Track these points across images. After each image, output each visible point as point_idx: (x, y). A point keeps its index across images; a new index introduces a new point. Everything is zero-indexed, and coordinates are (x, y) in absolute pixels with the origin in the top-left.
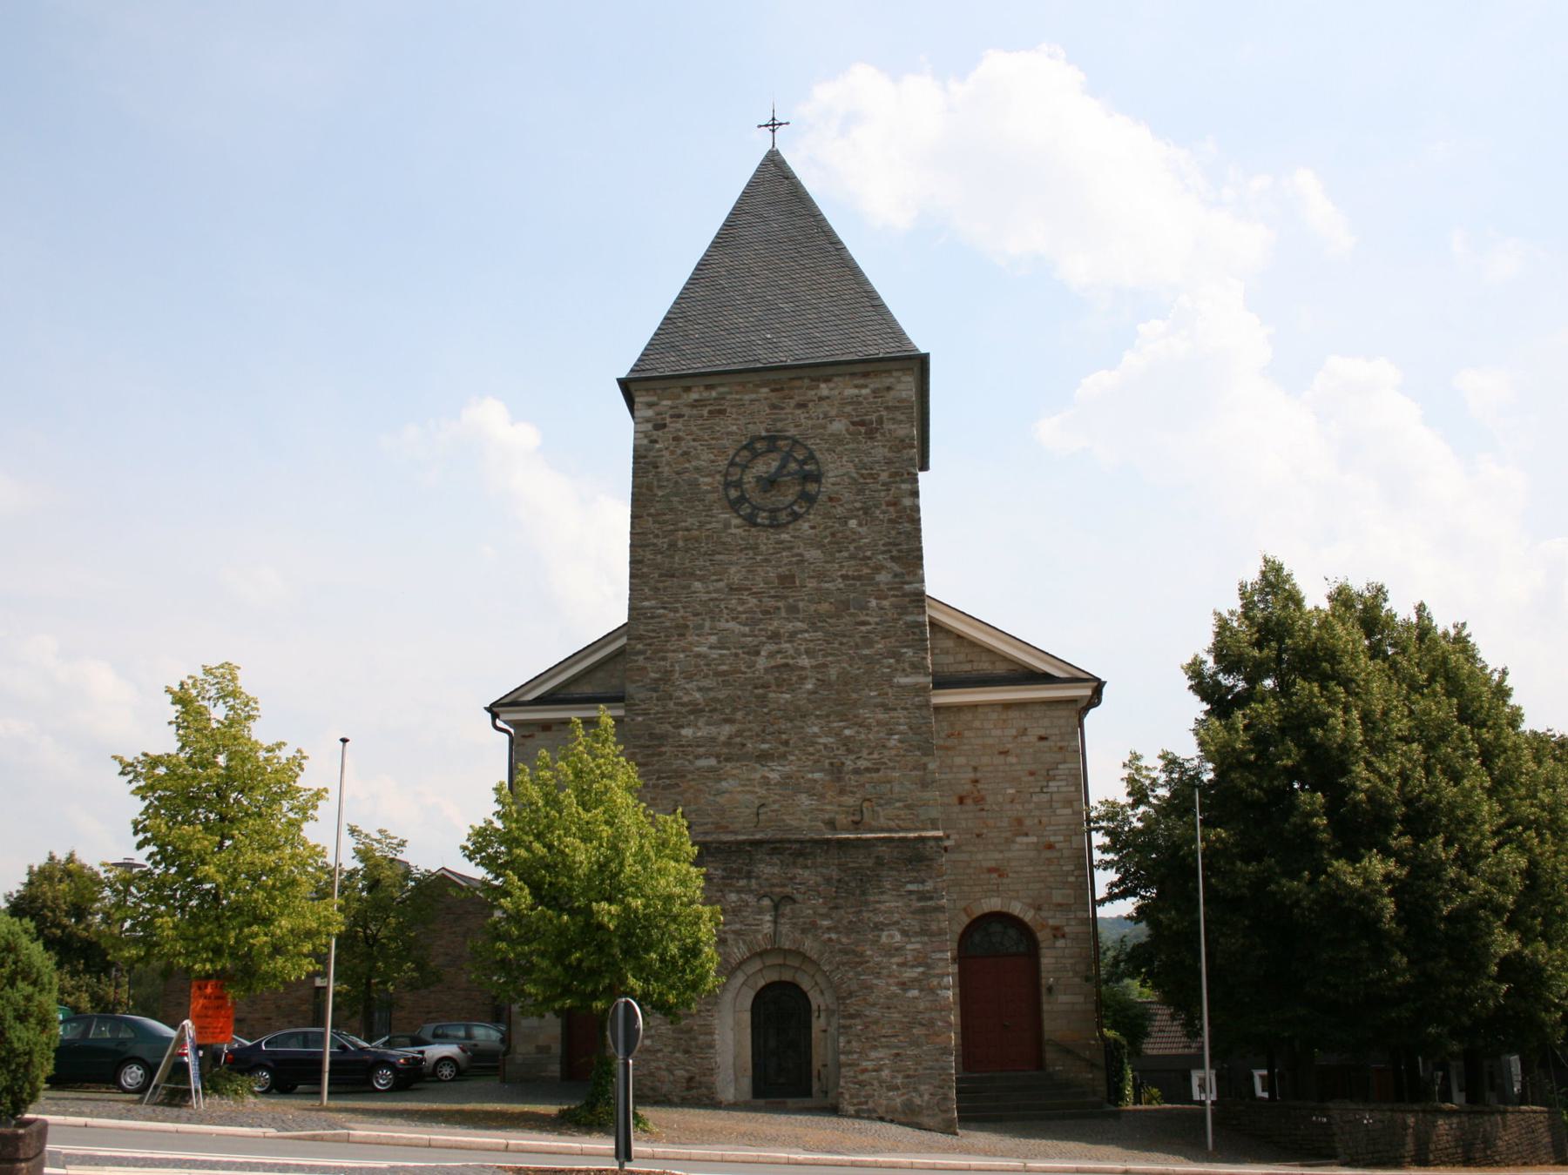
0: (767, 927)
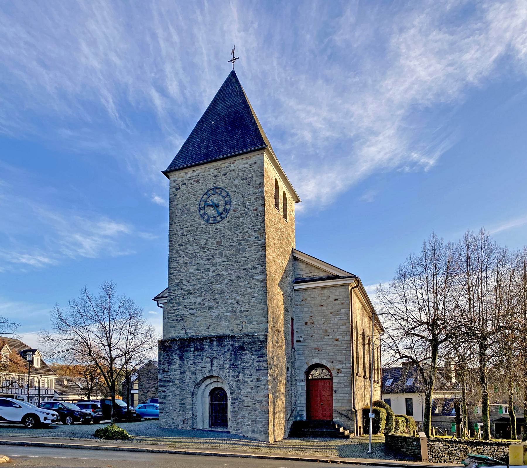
0: (208, 368)
